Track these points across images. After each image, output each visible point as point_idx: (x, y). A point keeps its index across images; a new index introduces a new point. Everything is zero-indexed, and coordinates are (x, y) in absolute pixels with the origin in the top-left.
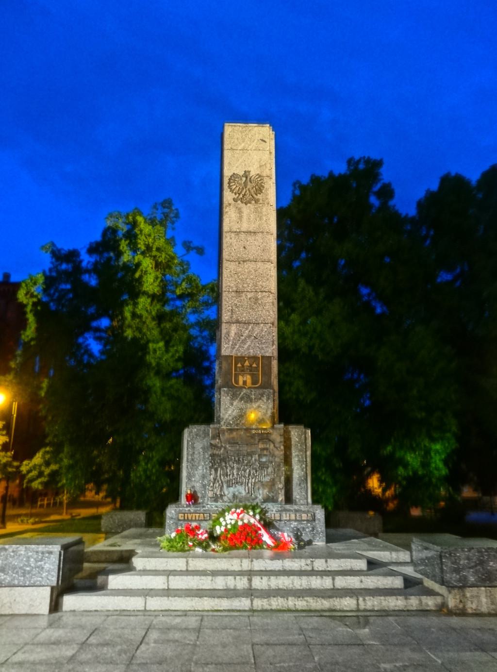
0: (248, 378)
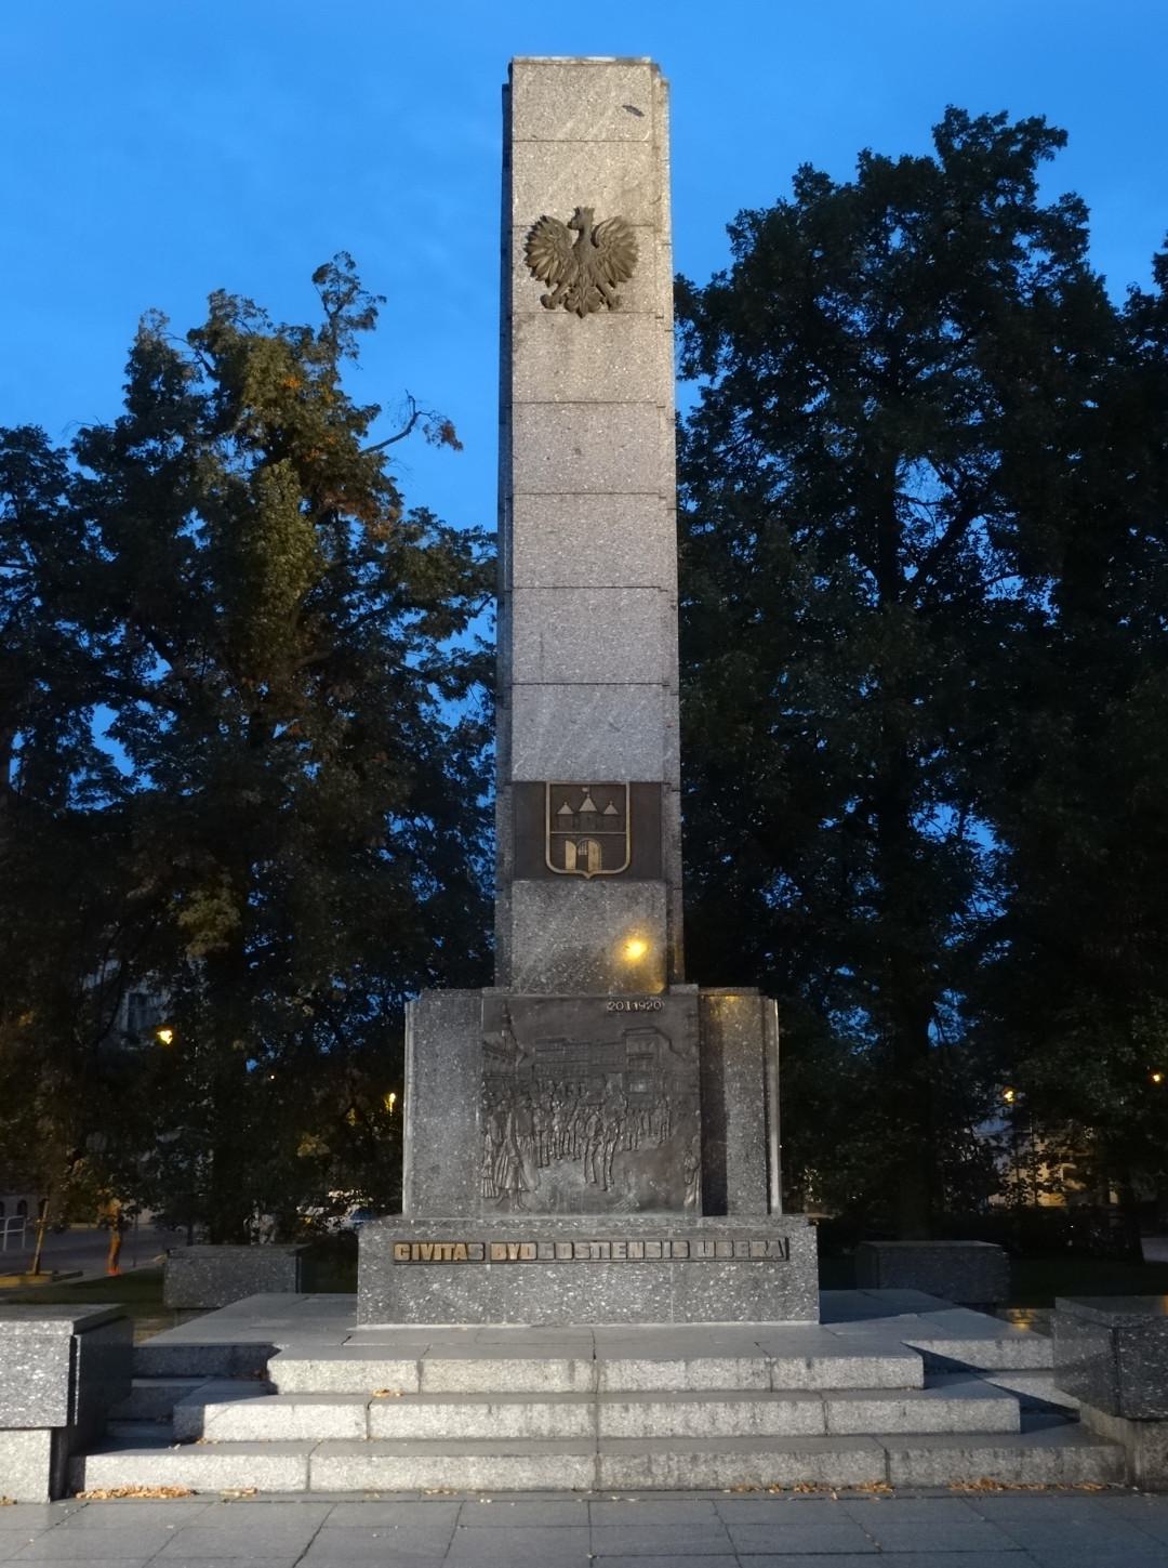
0: (594, 851)
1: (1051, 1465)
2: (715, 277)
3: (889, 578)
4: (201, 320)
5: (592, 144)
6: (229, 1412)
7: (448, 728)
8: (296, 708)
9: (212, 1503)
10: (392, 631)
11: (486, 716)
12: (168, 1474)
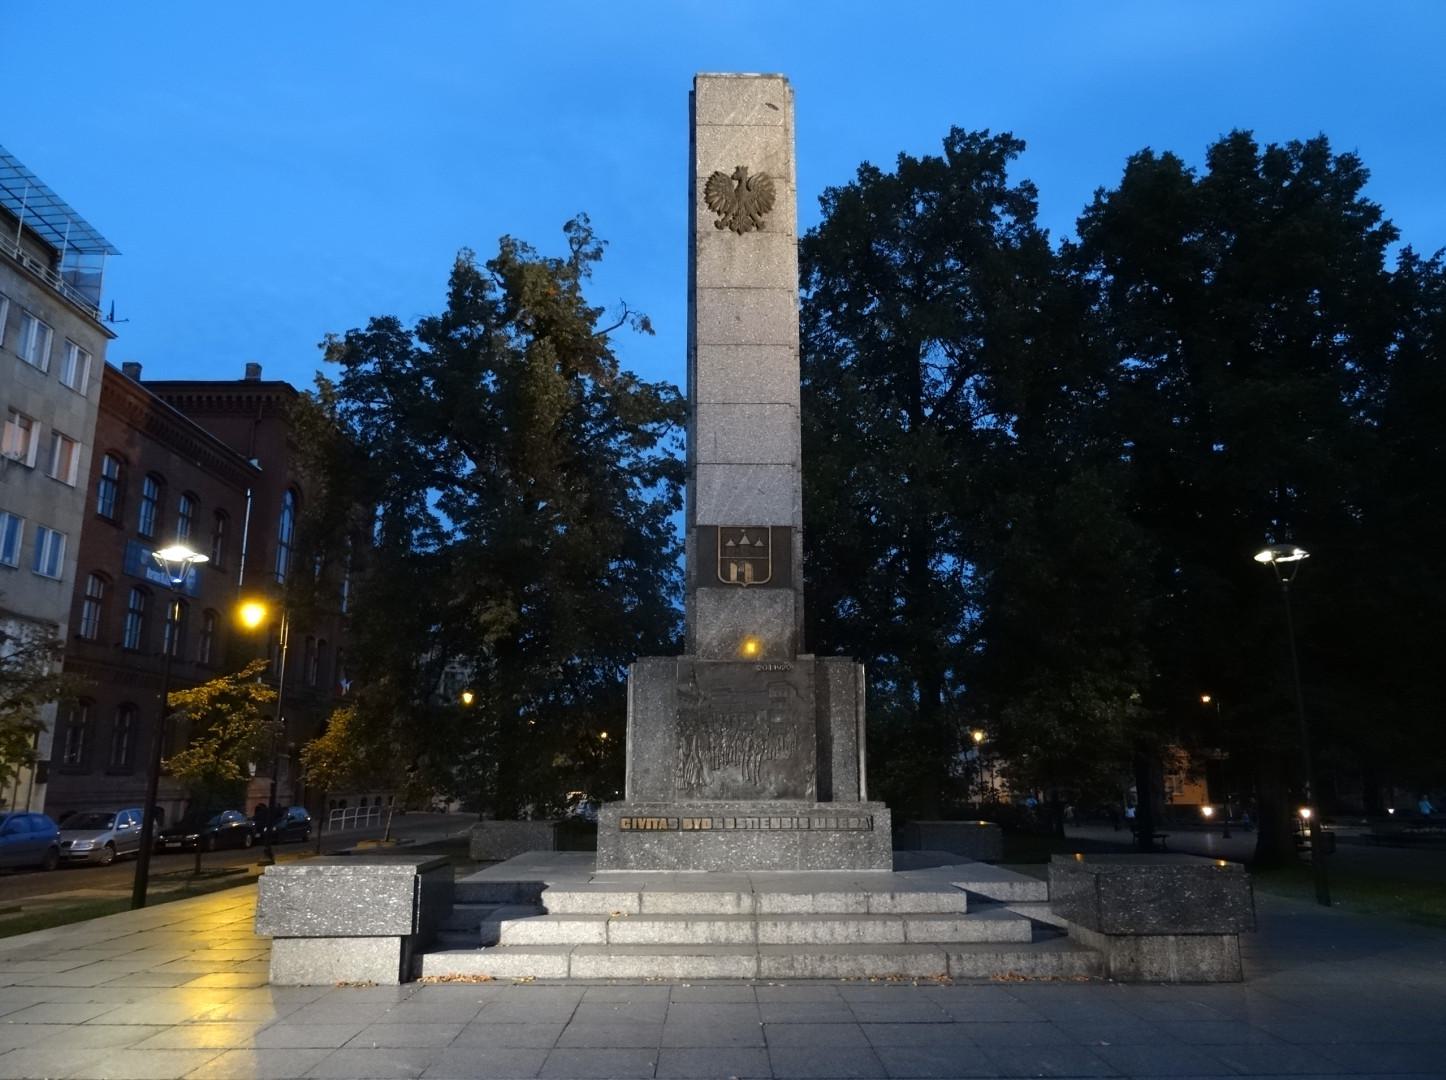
0: (748, 569)
1: (1055, 964)
2: (809, 231)
3: (917, 416)
4: (495, 254)
5: (746, 127)
6: (517, 926)
7: (646, 504)
8: (553, 491)
9: (506, 986)
10: (611, 445)
11: (669, 498)
12: (477, 966)
